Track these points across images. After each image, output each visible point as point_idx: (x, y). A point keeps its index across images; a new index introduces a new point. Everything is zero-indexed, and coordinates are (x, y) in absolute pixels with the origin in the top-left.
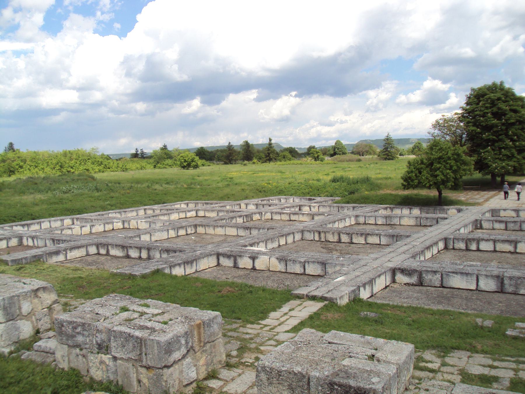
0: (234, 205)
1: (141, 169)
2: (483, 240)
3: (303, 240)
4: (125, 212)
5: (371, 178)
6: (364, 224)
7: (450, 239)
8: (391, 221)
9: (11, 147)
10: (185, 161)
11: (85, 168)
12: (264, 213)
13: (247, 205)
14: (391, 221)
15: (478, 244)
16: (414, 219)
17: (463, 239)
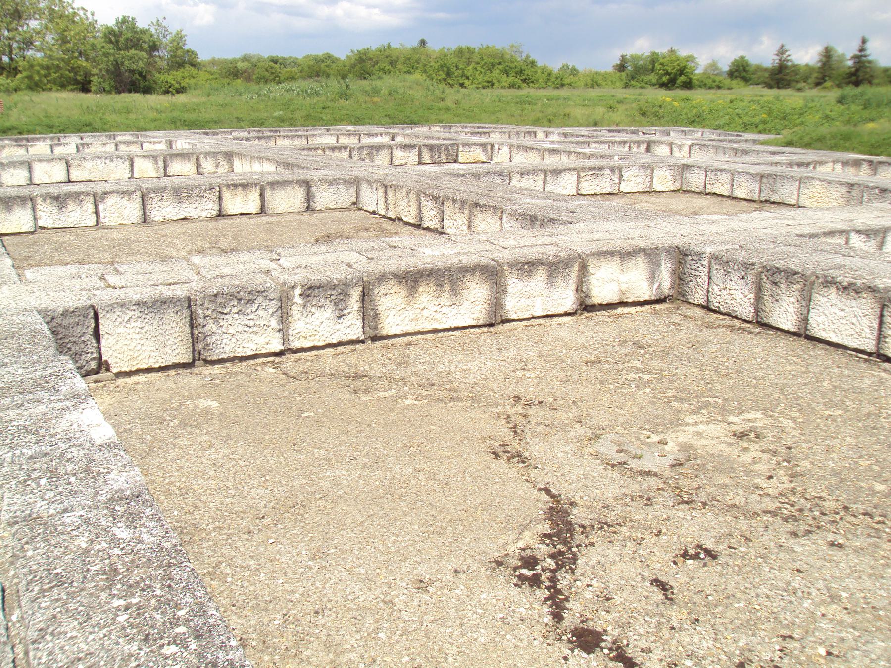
0: (518, 133)
1: (592, 87)
2: (829, 282)
3: (70, 181)
4: (314, 135)
5: (836, 51)
6: (700, 193)
7: (700, 255)
8: (774, 191)
9: (423, 42)
10: (667, 73)
11: (486, 78)
12: (496, 147)
13: (547, 134)
14: (774, 191)
15: (806, 300)
16: (844, 189)
17: (747, 266)
